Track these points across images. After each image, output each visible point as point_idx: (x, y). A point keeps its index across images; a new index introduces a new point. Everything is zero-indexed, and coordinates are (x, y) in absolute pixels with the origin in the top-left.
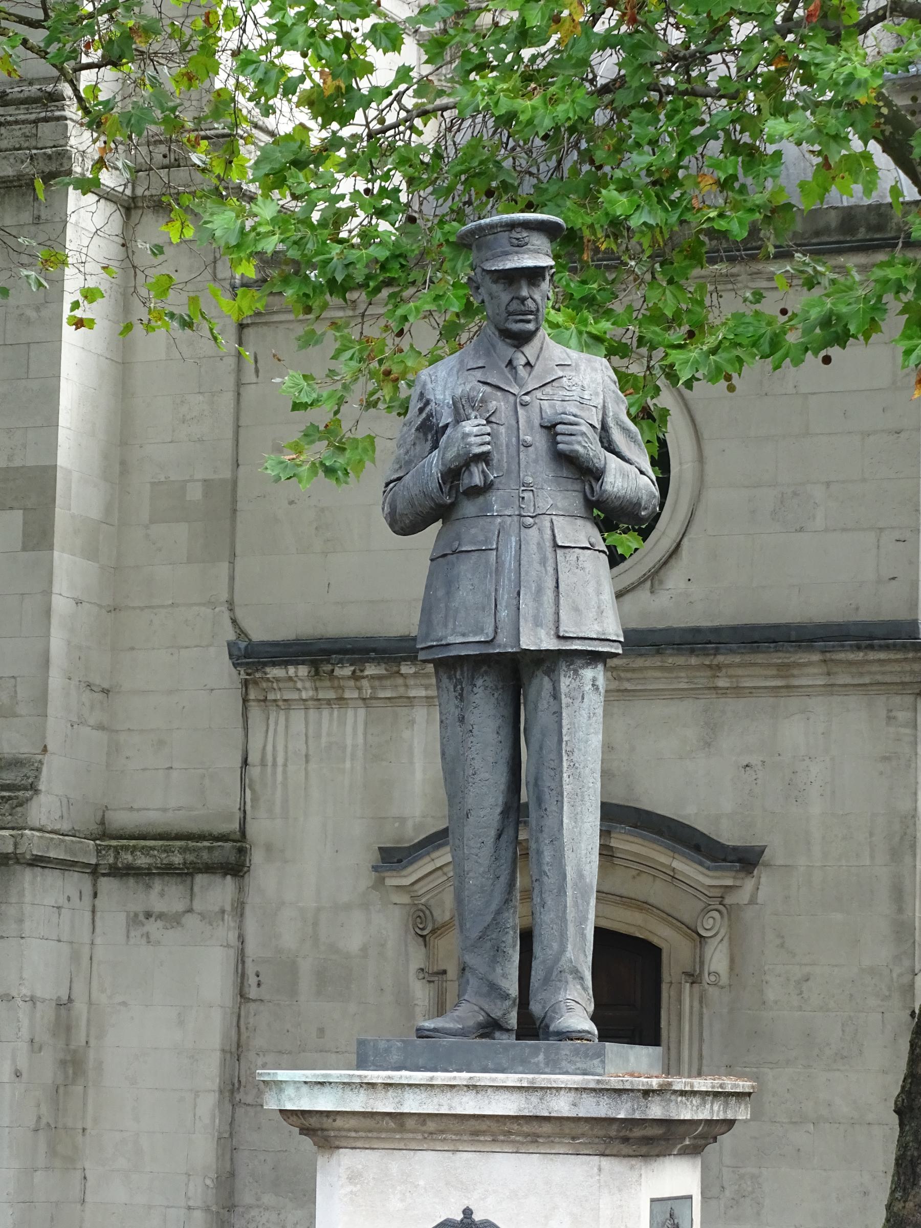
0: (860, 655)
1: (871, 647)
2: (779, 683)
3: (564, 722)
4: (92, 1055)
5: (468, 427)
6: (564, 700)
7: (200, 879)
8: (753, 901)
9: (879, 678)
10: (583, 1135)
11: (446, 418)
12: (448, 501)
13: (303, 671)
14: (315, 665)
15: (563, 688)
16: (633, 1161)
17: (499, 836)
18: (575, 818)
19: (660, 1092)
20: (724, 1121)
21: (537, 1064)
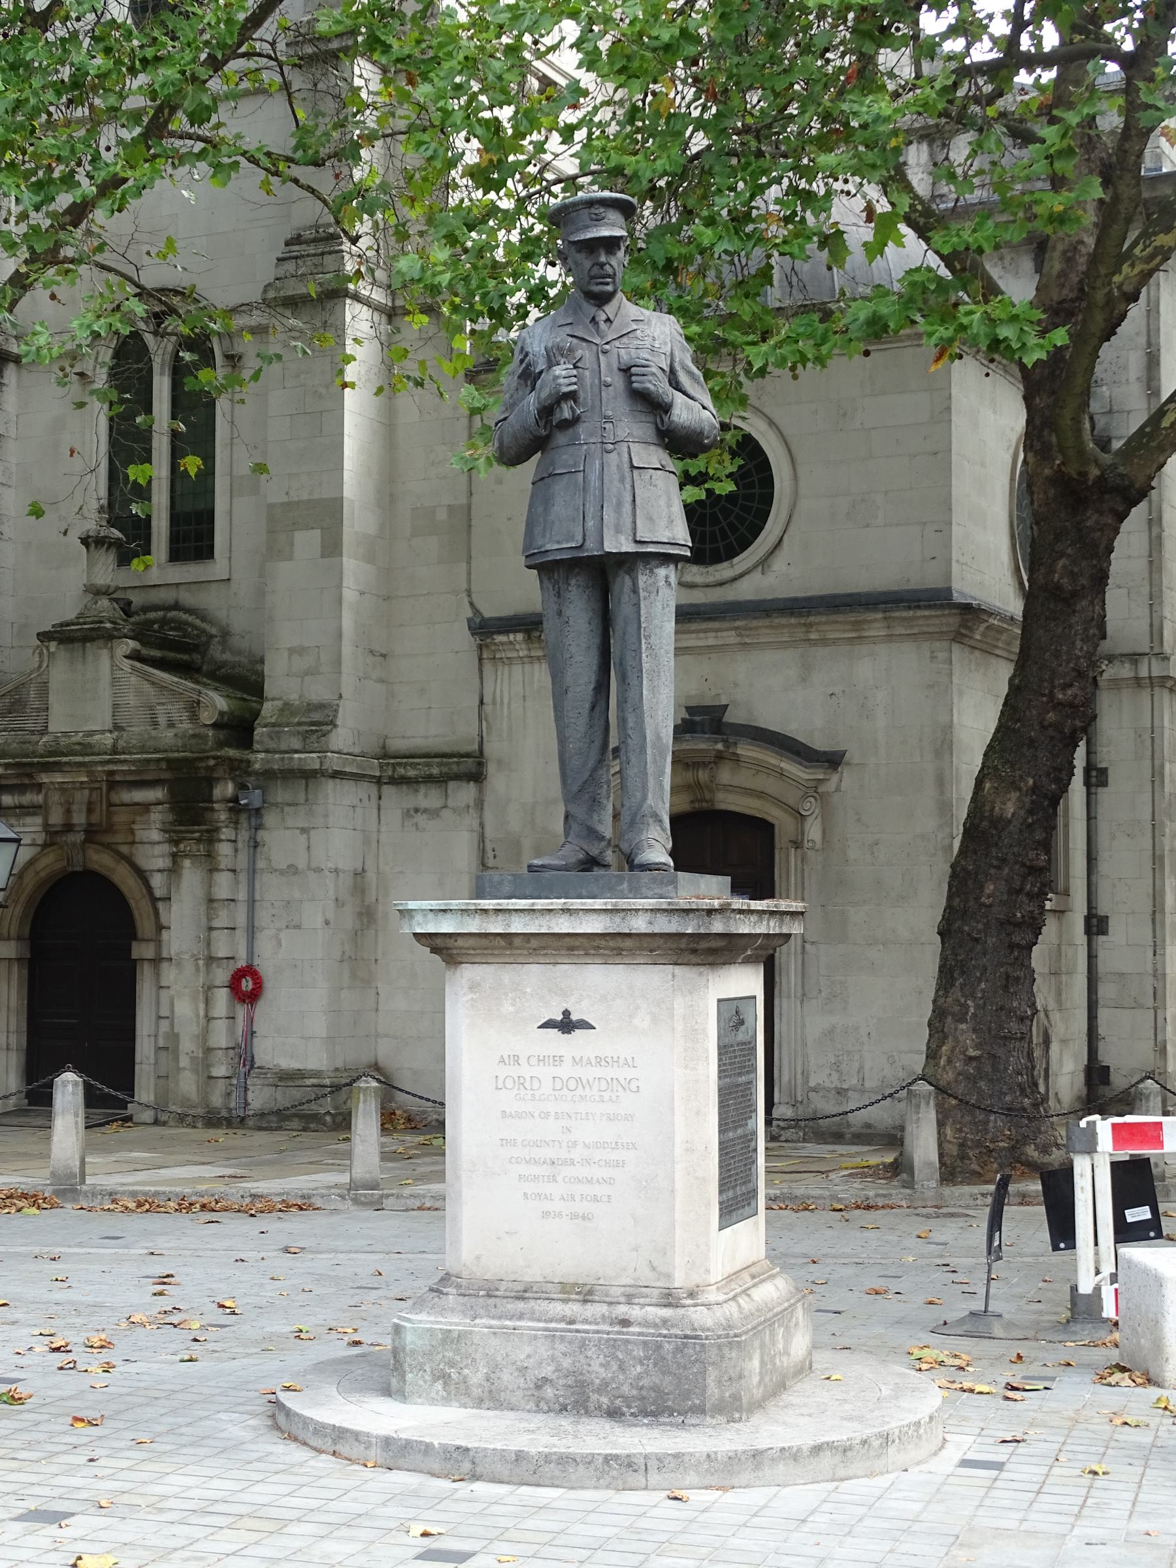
0: (911, 613)
1: (919, 607)
2: (854, 635)
3: (643, 612)
4: (380, 908)
5: (558, 371)
6: (642, 594)
7: (452, 785)
8: (838, 789)
9: (925, 629)
10: (659, 948)
11: (541, 365)
12: (543, 433)
13: (520, 636)
14: (528, 633)
15: (641, 584)
16: (702, 969)
17: (593, 708)
18: (654, 689)
19: (720, 911)
20: (781, 935)
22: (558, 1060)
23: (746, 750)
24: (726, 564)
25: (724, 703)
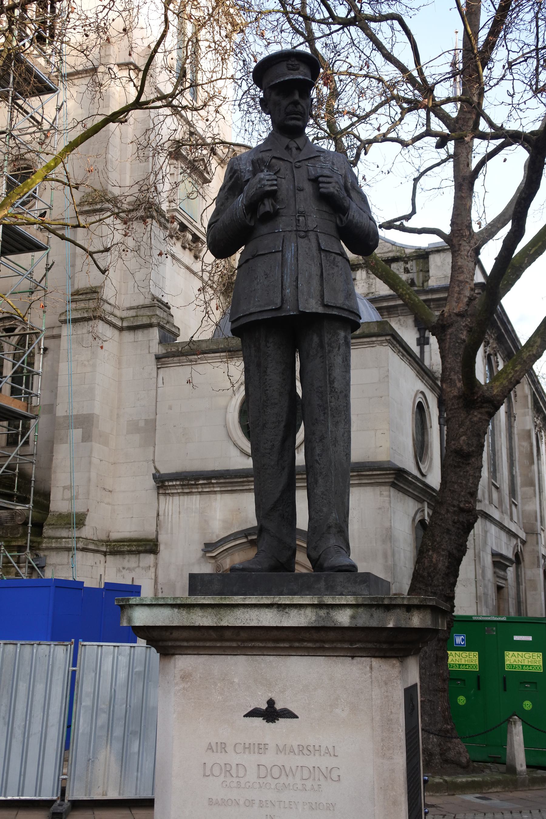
6: (327, 348)
7: (142, 555)
15: (326, 340)
22: (262, 748)
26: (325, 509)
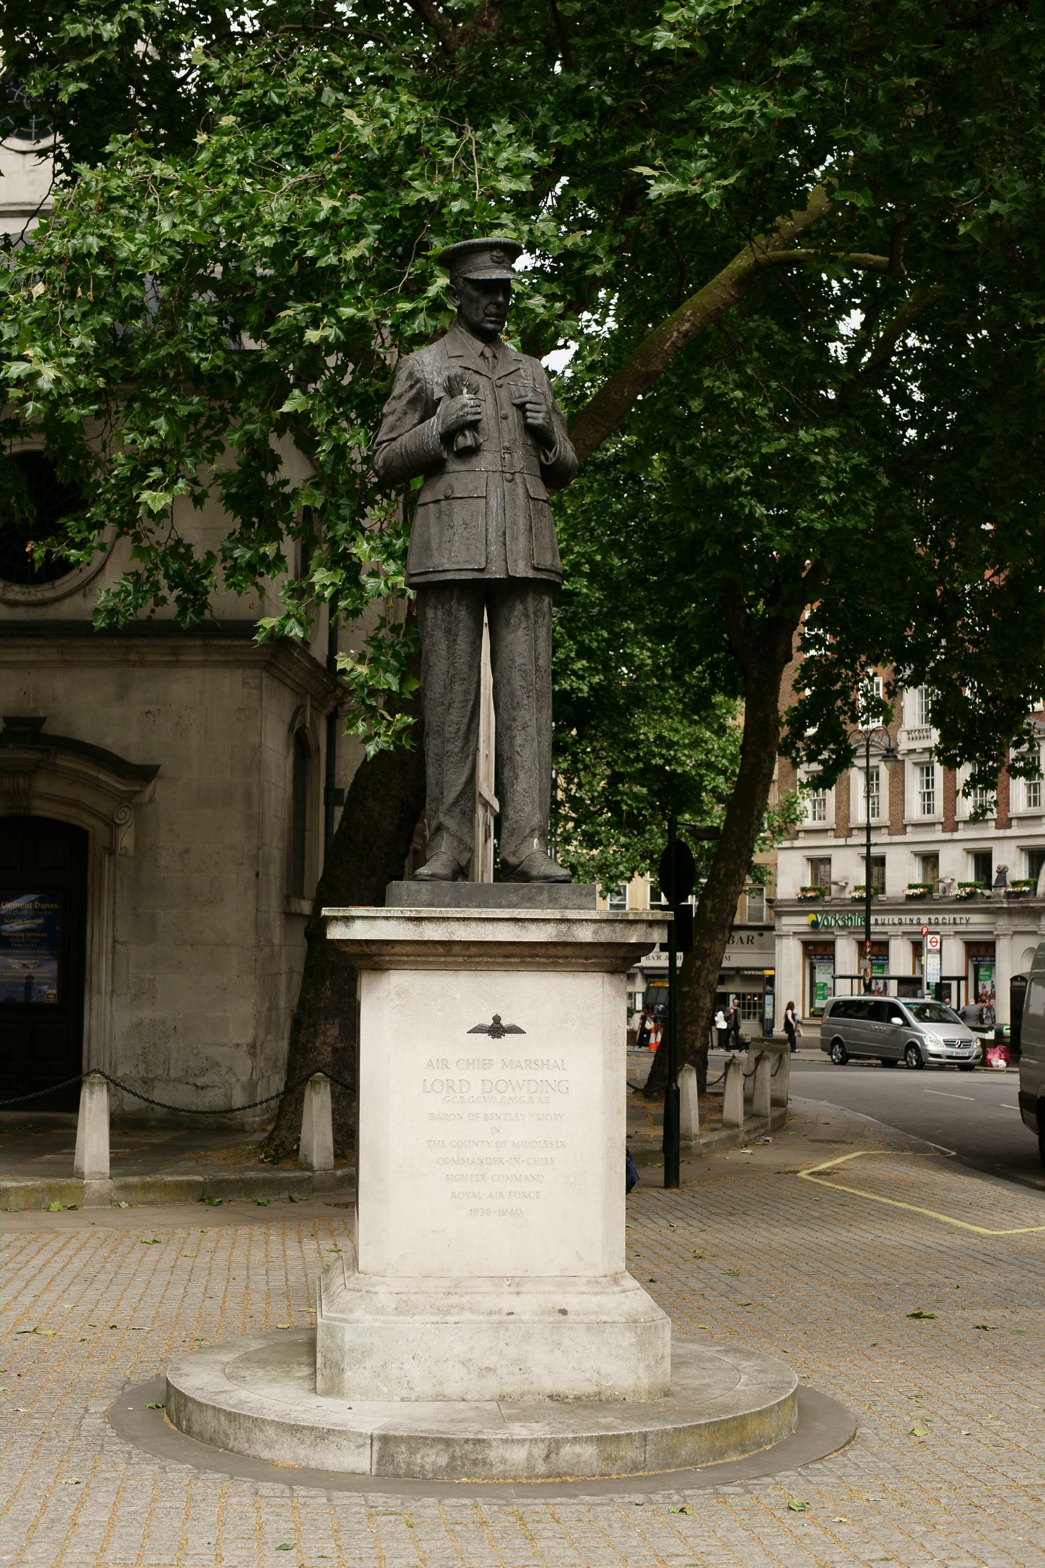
11: (439, 393)
21: (541, 902)
22: (487, 1064)
23: (65, 762)
24: (47, 586)
25: (42, 714)
26: (527, 809)
